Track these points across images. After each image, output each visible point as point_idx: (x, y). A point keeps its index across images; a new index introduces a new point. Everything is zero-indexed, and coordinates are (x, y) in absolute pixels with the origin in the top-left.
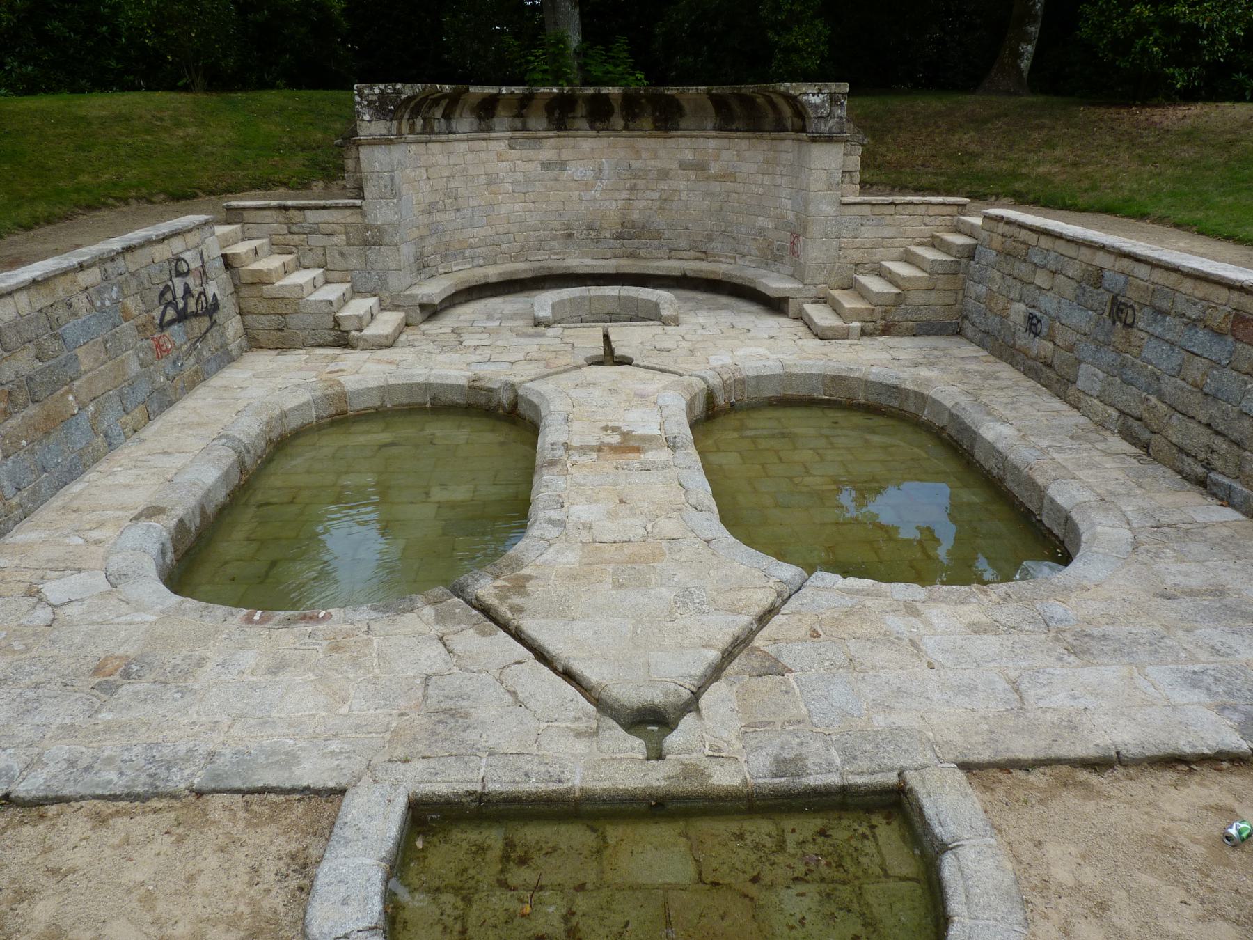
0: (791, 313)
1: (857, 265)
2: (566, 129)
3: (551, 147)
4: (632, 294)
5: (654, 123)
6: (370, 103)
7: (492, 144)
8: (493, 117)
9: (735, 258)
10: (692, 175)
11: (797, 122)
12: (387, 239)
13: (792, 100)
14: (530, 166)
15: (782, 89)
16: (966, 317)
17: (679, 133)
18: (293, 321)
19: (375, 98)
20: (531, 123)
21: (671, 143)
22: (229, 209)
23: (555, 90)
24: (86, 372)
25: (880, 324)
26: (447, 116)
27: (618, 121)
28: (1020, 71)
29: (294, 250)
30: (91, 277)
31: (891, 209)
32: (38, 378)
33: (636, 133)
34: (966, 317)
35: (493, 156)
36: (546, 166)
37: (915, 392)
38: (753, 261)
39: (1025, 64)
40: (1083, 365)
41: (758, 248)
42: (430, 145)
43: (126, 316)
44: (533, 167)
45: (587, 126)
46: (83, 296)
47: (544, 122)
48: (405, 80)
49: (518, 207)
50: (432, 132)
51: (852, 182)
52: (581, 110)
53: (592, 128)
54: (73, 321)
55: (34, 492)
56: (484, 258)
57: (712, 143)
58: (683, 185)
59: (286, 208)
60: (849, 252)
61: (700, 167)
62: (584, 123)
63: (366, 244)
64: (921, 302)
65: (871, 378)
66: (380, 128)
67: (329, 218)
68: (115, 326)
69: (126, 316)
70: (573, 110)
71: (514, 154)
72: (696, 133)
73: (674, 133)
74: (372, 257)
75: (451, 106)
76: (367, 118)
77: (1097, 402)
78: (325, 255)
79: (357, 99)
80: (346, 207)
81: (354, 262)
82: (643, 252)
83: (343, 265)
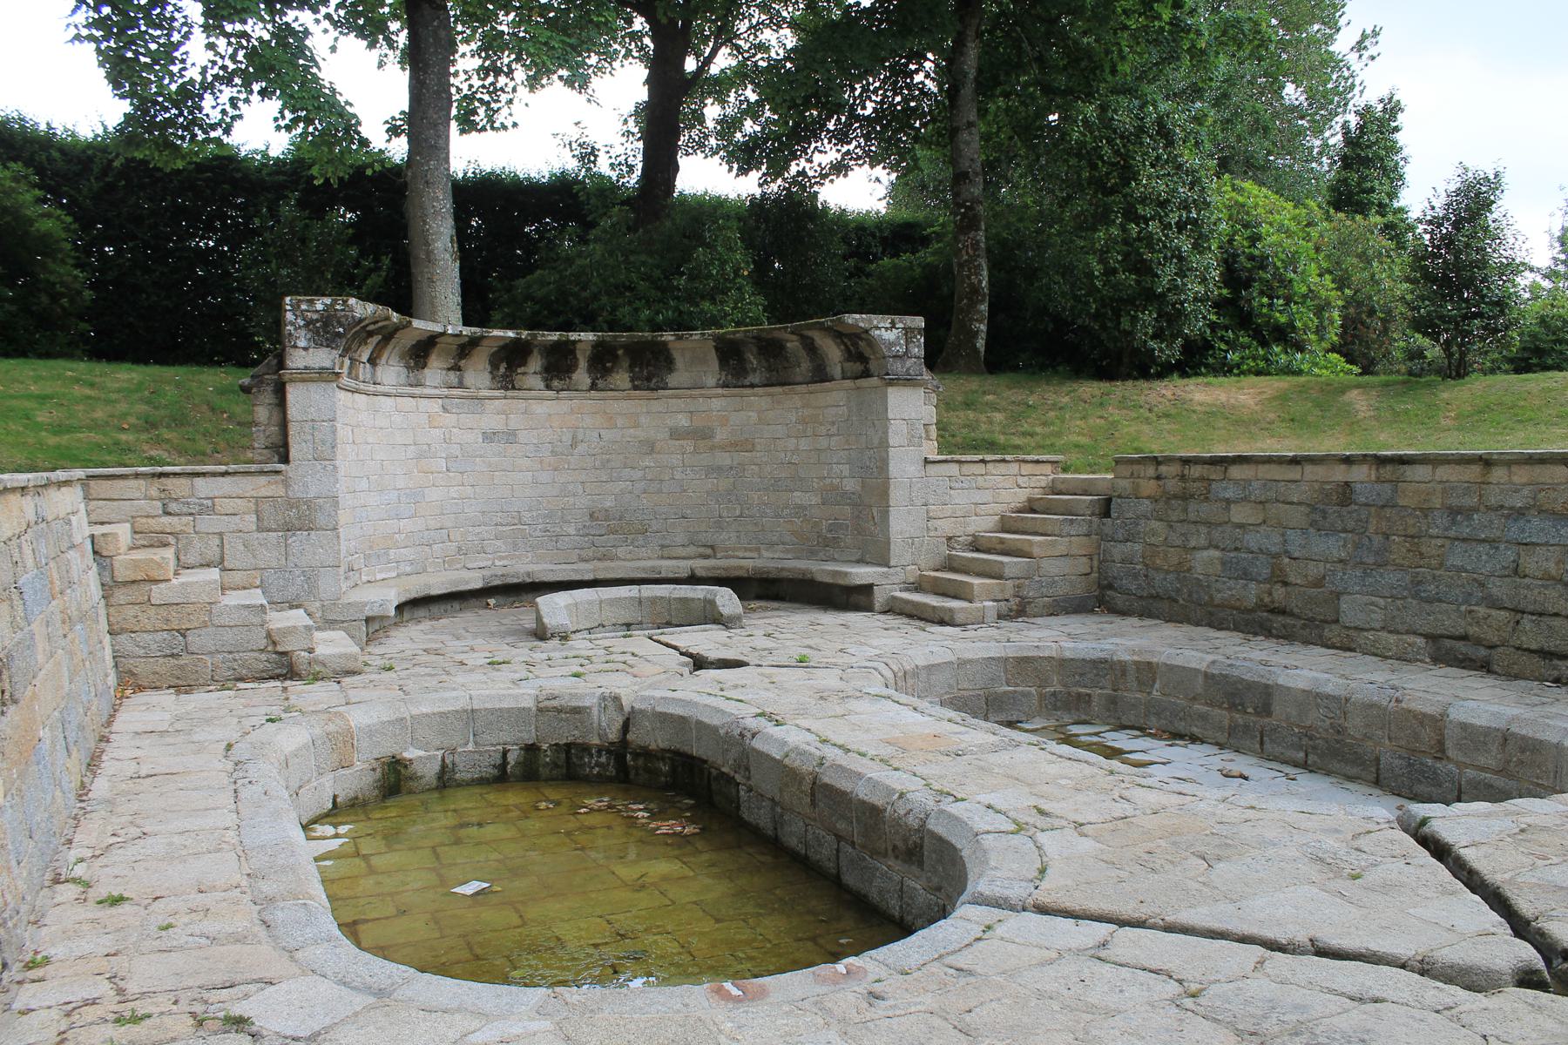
0: (877, 606)
1: (949, 539)
2: (514, 388)
5: (632, 380)
9: (758, 550)
10: (689, 445)
11: (862, 359)
12: (321, 519)
13: (862, 335)
16: (1110, 587)
19: (315, 316)
21: (656, 406)
23: (511, 334)
25: (1014, 602)
27: (582, 376)
28: (976, 351)
29: (171, 540)
31: (980, 469)
34: (1110, 587)
37: (1136, 663)
38: (788, 551)
39: (981, 343)
40: (1344, 598)
41: (793, 533)
44: (474, 438)
45: (542, 385)
52: (535, 363)
53: (548, 387)
56: (411, 563)
57: (716, 403)
60: (939, 522)
61: (700, 435)
62: (537, 381)
63: (289, 528)
64: (1056, 571)
66: (322, 357)
67: (230, 496)
70: (524, 363)
71: (450, 419)
73: (661, 392)
77: (1384, 634)
78: (222, 546)
82: (621, 552)
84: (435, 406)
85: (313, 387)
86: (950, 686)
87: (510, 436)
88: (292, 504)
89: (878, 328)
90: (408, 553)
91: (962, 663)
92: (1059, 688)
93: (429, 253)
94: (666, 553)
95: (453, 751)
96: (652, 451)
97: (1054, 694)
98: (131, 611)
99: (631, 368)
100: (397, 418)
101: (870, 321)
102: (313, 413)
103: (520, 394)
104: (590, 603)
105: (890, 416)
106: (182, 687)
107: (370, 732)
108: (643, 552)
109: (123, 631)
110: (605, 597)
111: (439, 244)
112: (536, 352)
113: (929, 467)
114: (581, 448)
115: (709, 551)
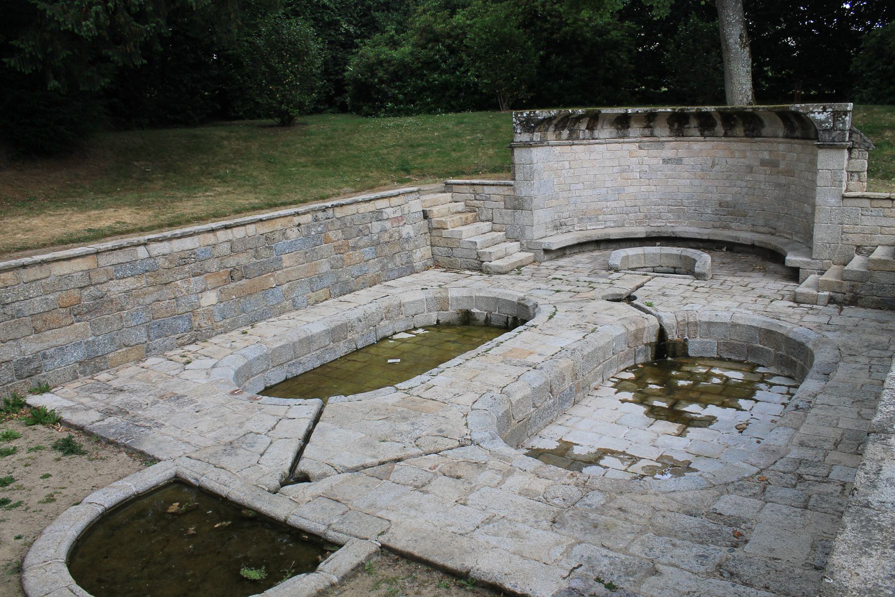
1: (858, 247)
2: (683, 136)
3: (672, 148)
4: (689, 254)
6: (521, 122)
7: (626, 146)
8: (628, 127)
9: (792, 234)
10: (768, 170)
12: (526, 206)
14: (654, 161)
15: (793, 109)
17: (760, 139)
18: (456, 252)
20: (657, 131)
21: (755, 147)
22: (447, 184)
24: (286, 267)
25: (848, 295)
26: (591, 128)
30: (308, 218)
32: (252, 267)
33: (732, 139)
35: (626, 153)
36: (666, 161)
38: (801, 238)
42: (574, 147)
43: (327, 241)
44: (657, 162)
45: (698, 134)
46: (295, 229)
47: (667, 131)
48: (542, 107)
49: (643, 189)
50: (578, 138)
51: (859, 180)
52: (694, 123)
53: (702, 135)
54: (284, 241)
55: (234, 321)
57: (782, 147)
58: (762, 177)
59: (474, 184)
60: (850, 235)
61: (772, 164)
63: (515, 208)
65: (791, 335)
67: (494, 193)
68: (315, 245)
69: (327, 241)
70: (687, 123)
71: (643, 153)
72: (771, 139)
74: (517, 216)
75: (593, 121)
76: (519, 131)
79: (514, 120)
80: (505, 185)
81: (508, 219)
82: (733, 225)
83: (501, 221)
84: (634, 147)
85: (523, 150)
86: (725, 336)
87: (679, 161)
88: (517, 198)
89: (812, 112)
90: (614, 217)
91: (734, 325)
92: (784, 353)
93: (727, 46)
94: (755, 229)
95: (491, 313)
96: (751, 172)
97: (781, 356)
98: (437, 239)
99: (744, 125)
100: (608, 154)
101: (808, 108)
102: (523, 161)
103: (685, 138)
104: (654, 254)
105: (819, 167)
106: (449, 268)
107: (457, 299)
108: (744, 227)
109: (435, 246)
110: (663, 252)
111: (731, 41)
112: (692, 117)
113: (845, 200)
114: (717, 168)
115: (773, 231)
